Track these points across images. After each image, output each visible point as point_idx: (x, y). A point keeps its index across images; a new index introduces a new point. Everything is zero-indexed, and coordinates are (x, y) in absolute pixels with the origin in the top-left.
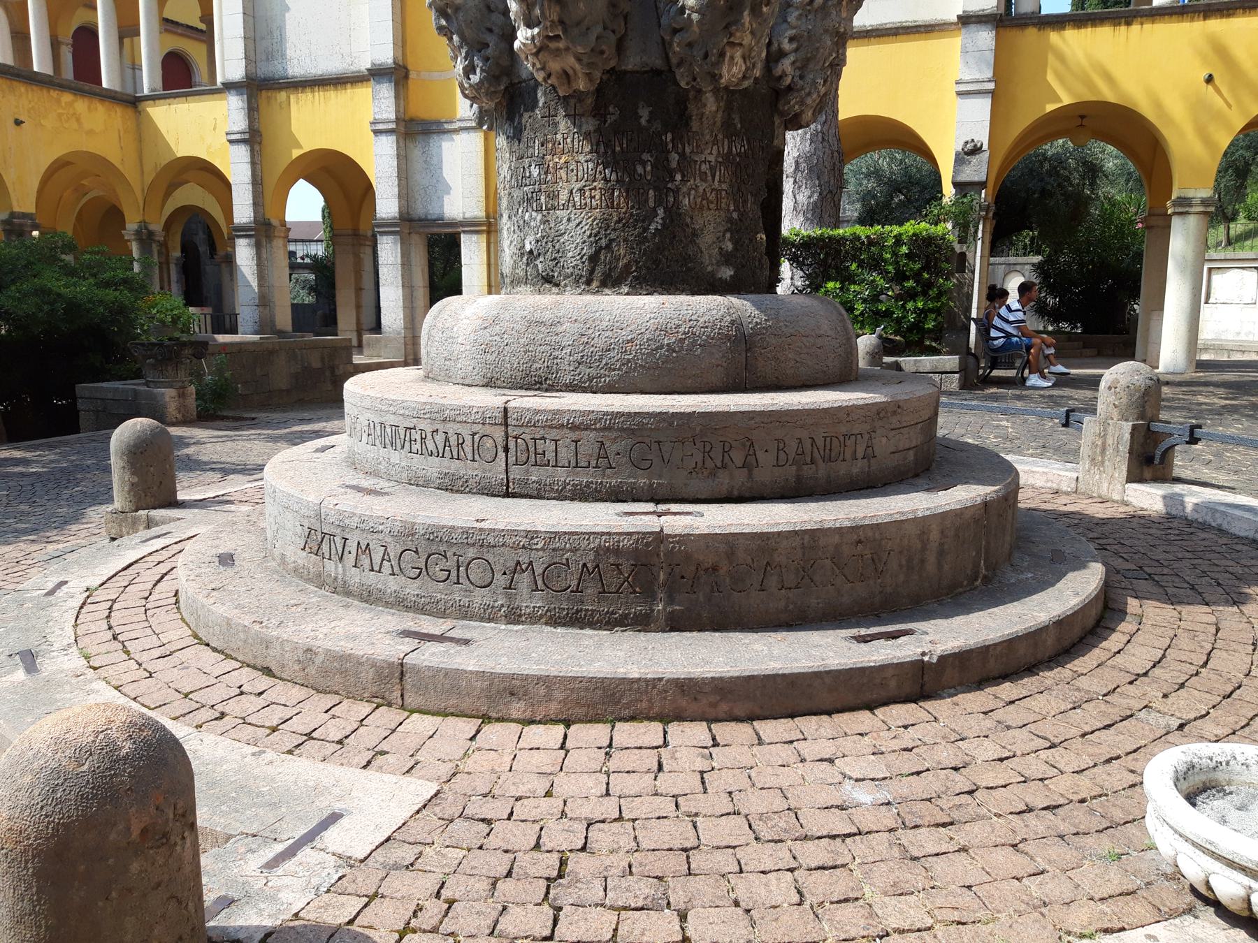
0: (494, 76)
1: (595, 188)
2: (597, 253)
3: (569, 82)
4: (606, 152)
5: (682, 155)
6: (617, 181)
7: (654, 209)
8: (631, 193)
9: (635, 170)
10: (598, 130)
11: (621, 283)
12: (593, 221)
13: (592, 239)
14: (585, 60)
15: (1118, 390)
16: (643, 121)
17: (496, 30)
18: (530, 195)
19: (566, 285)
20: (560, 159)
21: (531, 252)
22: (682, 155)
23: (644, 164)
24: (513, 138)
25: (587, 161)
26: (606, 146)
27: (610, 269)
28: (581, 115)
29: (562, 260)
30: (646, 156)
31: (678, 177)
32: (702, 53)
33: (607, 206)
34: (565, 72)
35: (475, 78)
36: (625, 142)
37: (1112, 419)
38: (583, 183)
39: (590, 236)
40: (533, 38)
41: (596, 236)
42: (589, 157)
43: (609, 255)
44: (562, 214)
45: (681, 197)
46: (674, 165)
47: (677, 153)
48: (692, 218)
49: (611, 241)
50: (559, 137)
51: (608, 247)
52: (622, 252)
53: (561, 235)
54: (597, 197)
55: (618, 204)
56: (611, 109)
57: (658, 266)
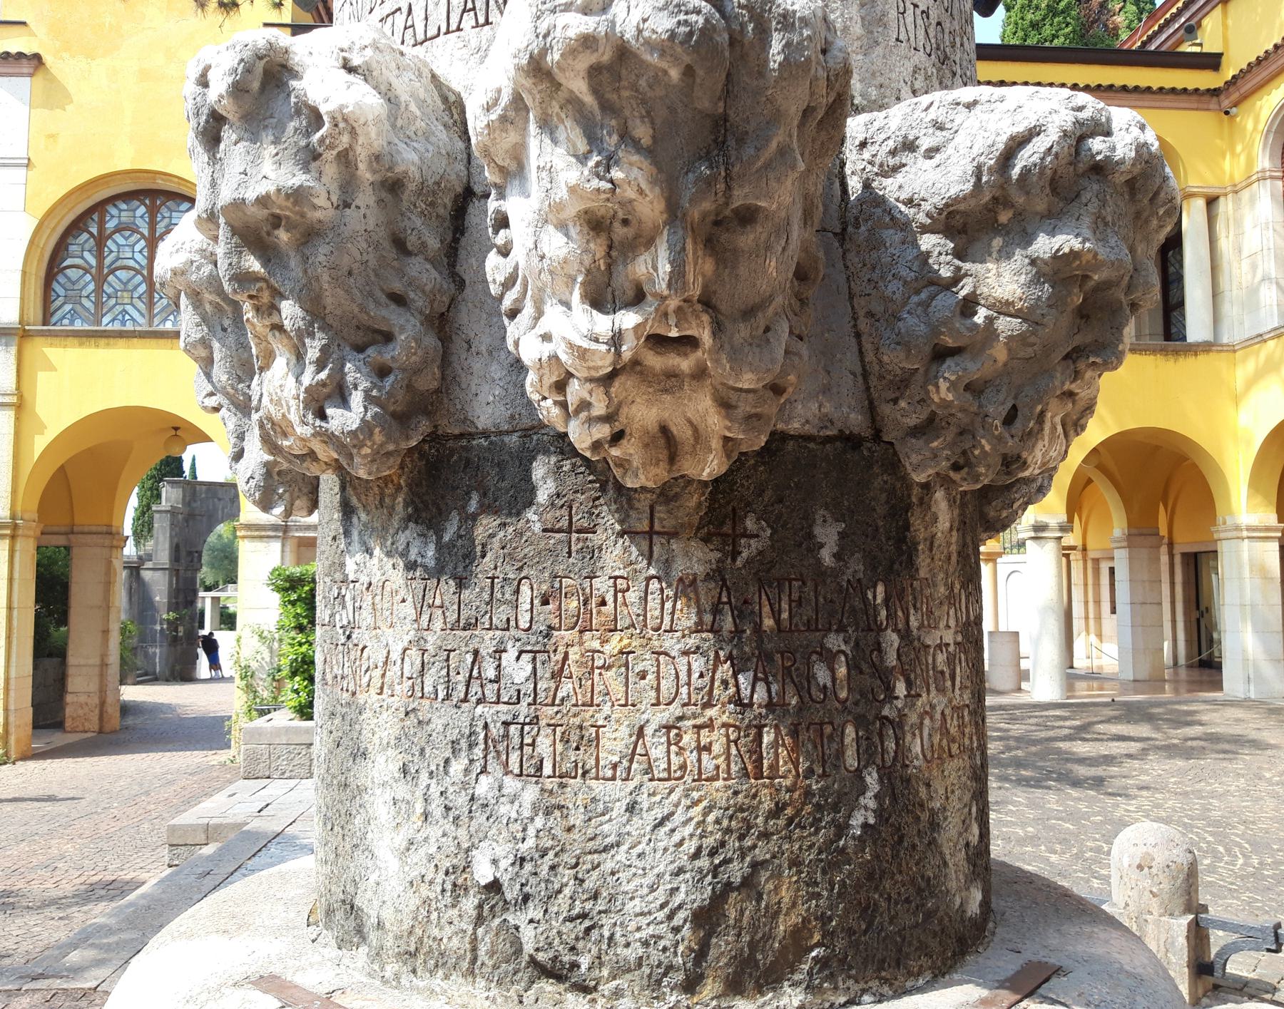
0: (394, 415)
1: (710, 725)
2: (719, 899)
3: (672, 459)
4: (738, 632)
5: (906, 635)
6: (770, 705)
7: (858, 774)
8: (803, 736)
9: (810, 678)
10: (717, 575)
11: (779, 980)
12: (705, 814)
13: (704, 863)
14: (745, 407)
15: (1154, 871)
16: (826, 556)
17: (418, 301)
18: (496, 730)
19: (617, 994)
20: (604, 642)
21: (494, 887)
22: (906, 635)
23: (830, 659)
24: (436, 572)
25: (686, 653)
26: (739, 615)
27: (753, 945)
28: (672, 535)
29: (606, 921)
30: (834, 642)
31: (901, 689)
32: (1004, 410)
33: (745, 774)
34: (664, 430)
35: (345, 419)
36: (785, 606)
37: (1150, 913)
38: (676, 710)
39: (696, 855)
40: (616, 339)
41: (713, 853)
42: (692, 641)
43: (750, 907)
44: (617, 792)
45: (908, 738)
46: (891, 660)
47: (896, 630)
48: (928, 785)
49: (756, 866)
50: (602, 585)
51: (748, 883)
52: (786, 895)
53: (606, 849)
54: (717, 748)
55: (774, 767)
56: (750, 524)
57: (870, 925)
